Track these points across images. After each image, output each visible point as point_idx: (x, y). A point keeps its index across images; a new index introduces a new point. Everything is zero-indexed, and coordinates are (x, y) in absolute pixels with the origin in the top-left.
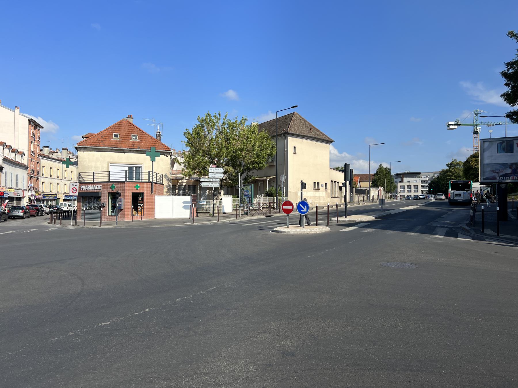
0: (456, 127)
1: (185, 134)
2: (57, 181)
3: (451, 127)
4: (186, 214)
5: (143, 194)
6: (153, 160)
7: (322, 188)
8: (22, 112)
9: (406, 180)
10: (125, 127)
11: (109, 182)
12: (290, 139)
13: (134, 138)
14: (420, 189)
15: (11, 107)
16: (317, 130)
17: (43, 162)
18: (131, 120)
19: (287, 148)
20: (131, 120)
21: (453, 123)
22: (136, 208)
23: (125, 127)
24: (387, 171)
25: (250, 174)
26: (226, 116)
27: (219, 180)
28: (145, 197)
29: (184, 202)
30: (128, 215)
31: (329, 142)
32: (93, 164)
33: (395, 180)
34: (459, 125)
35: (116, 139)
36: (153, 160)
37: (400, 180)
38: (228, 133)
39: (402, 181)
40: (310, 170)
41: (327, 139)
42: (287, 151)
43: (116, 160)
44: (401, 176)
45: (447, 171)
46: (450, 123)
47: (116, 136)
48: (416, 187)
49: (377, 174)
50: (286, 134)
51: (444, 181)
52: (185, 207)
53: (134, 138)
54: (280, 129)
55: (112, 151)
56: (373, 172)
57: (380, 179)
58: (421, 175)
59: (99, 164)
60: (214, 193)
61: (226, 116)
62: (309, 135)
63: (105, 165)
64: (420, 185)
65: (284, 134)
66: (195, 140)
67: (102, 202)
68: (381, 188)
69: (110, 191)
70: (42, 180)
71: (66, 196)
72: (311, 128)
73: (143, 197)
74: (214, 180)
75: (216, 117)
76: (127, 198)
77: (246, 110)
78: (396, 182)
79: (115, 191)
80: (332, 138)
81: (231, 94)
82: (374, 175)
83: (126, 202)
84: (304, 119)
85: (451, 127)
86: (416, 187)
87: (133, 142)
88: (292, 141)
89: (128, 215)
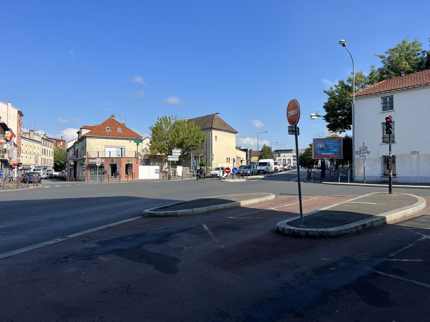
0: (316, 117)
1: (150, 128)
2: (30, 156)
3: (313, 117)
4: (157, 177)
5: (132, 164)
6: (138, 145)
7: (232, 161)
8: (14, 106)
9: (282, 155)
10: (111, 122)
11: (110, 158)
12: (213, 131)
13: (119, 130)
14: (292, 162)
15: (6, 102)
16: (228, 125)
17: (23, 141)
18: (114, 118)
19: (212, 137)
20: (114, 118)
21: (314, 114)
22: (127, 173)
23: (111, 122)
24: (269, 149)
25: (189, 152)
26: (176, 117)
27: (178, 157)
28: (133, 167)
29: (156, 170)
30: (124, 178)
31: (236, 133)
32: (96, 146)
33: (274, 155)
34: (318, 116)
35: (109, 131)
36: (138, 145)
37: (278, 155)
38: (177, 127)
39: (280, 156)
40: (225, 150)
41: (234, 131)
42: (212, 139)
43: (110, 144)
44: (279, 152)
45: (309, 149)
46: (312, 115)
47: (108, 129)
48: (289, 160)
49: (262, 151)
50: (211, 128)
51: (307, 156)
52: (156, 173)
53: (119, 130)
54: (208, 124)
55: (107, 138)
56: (260, 149)
57: (264, 154)
58: (292, 152)
59: (99, 146)
60: (174, 164)
61: (176, 117)
62: (224, 129)
63: (103, 147)
64: (292, 158)
65: (210, 128)
66: (156, 132)
67: (105, 169)
68: (178, 160)
69: (111, 163)
70: (22, 154)
71: (35, 167)
72: (225, 124)
73: (132, 167)
74: (175, 157)
75: (170, 118)
76: (122, 167)
77: (183, 110)
78: (275, 157)
79: (114, 163)
80: (237, 130)
81: (138, 79)
82: (260, 152)
83: (122, 170)
84: (220, 119)
85: (313, 117)
86: (289, 160)
87: (119, 133)
88: (214, 133)
89: (124, 178)
